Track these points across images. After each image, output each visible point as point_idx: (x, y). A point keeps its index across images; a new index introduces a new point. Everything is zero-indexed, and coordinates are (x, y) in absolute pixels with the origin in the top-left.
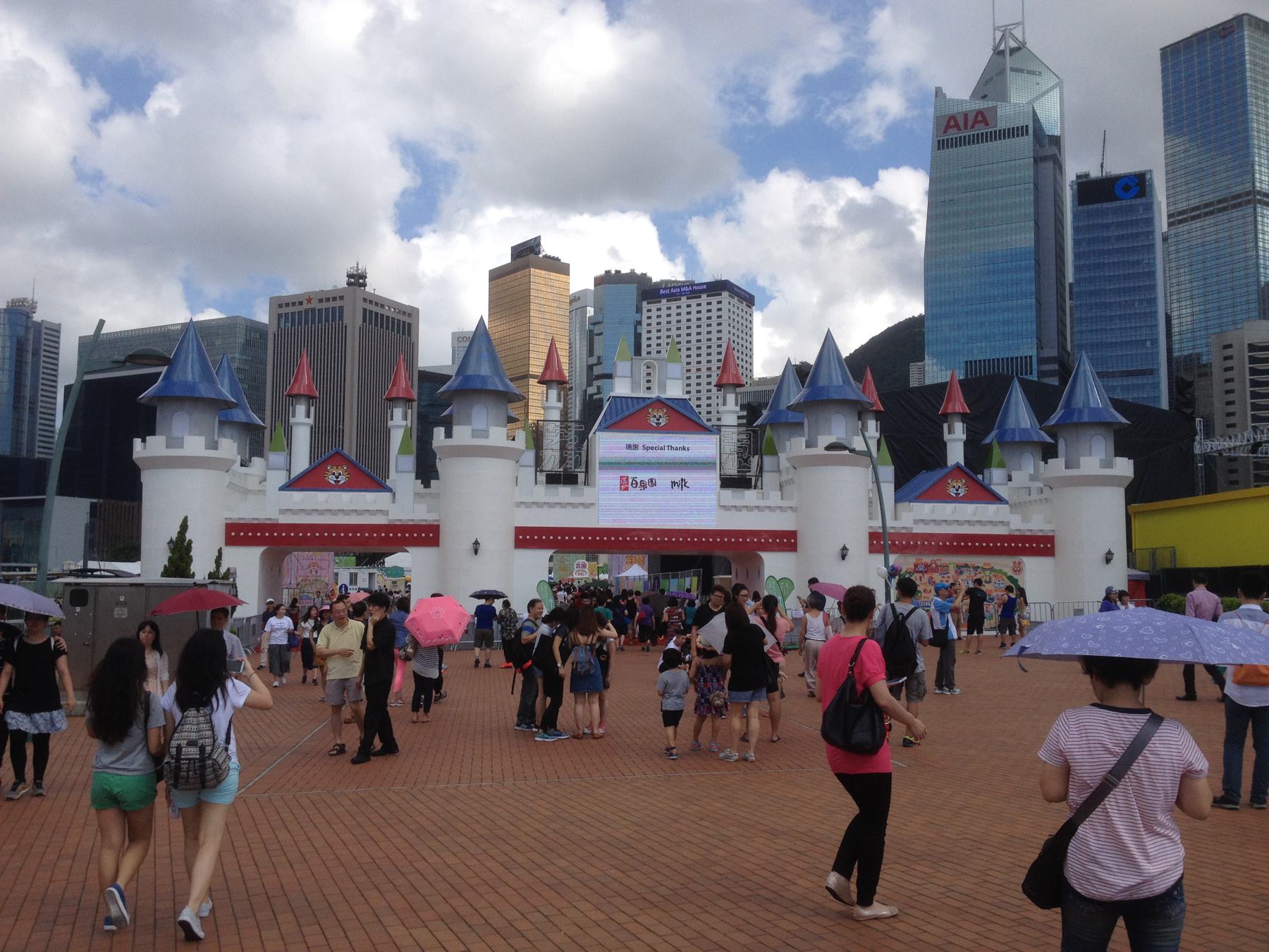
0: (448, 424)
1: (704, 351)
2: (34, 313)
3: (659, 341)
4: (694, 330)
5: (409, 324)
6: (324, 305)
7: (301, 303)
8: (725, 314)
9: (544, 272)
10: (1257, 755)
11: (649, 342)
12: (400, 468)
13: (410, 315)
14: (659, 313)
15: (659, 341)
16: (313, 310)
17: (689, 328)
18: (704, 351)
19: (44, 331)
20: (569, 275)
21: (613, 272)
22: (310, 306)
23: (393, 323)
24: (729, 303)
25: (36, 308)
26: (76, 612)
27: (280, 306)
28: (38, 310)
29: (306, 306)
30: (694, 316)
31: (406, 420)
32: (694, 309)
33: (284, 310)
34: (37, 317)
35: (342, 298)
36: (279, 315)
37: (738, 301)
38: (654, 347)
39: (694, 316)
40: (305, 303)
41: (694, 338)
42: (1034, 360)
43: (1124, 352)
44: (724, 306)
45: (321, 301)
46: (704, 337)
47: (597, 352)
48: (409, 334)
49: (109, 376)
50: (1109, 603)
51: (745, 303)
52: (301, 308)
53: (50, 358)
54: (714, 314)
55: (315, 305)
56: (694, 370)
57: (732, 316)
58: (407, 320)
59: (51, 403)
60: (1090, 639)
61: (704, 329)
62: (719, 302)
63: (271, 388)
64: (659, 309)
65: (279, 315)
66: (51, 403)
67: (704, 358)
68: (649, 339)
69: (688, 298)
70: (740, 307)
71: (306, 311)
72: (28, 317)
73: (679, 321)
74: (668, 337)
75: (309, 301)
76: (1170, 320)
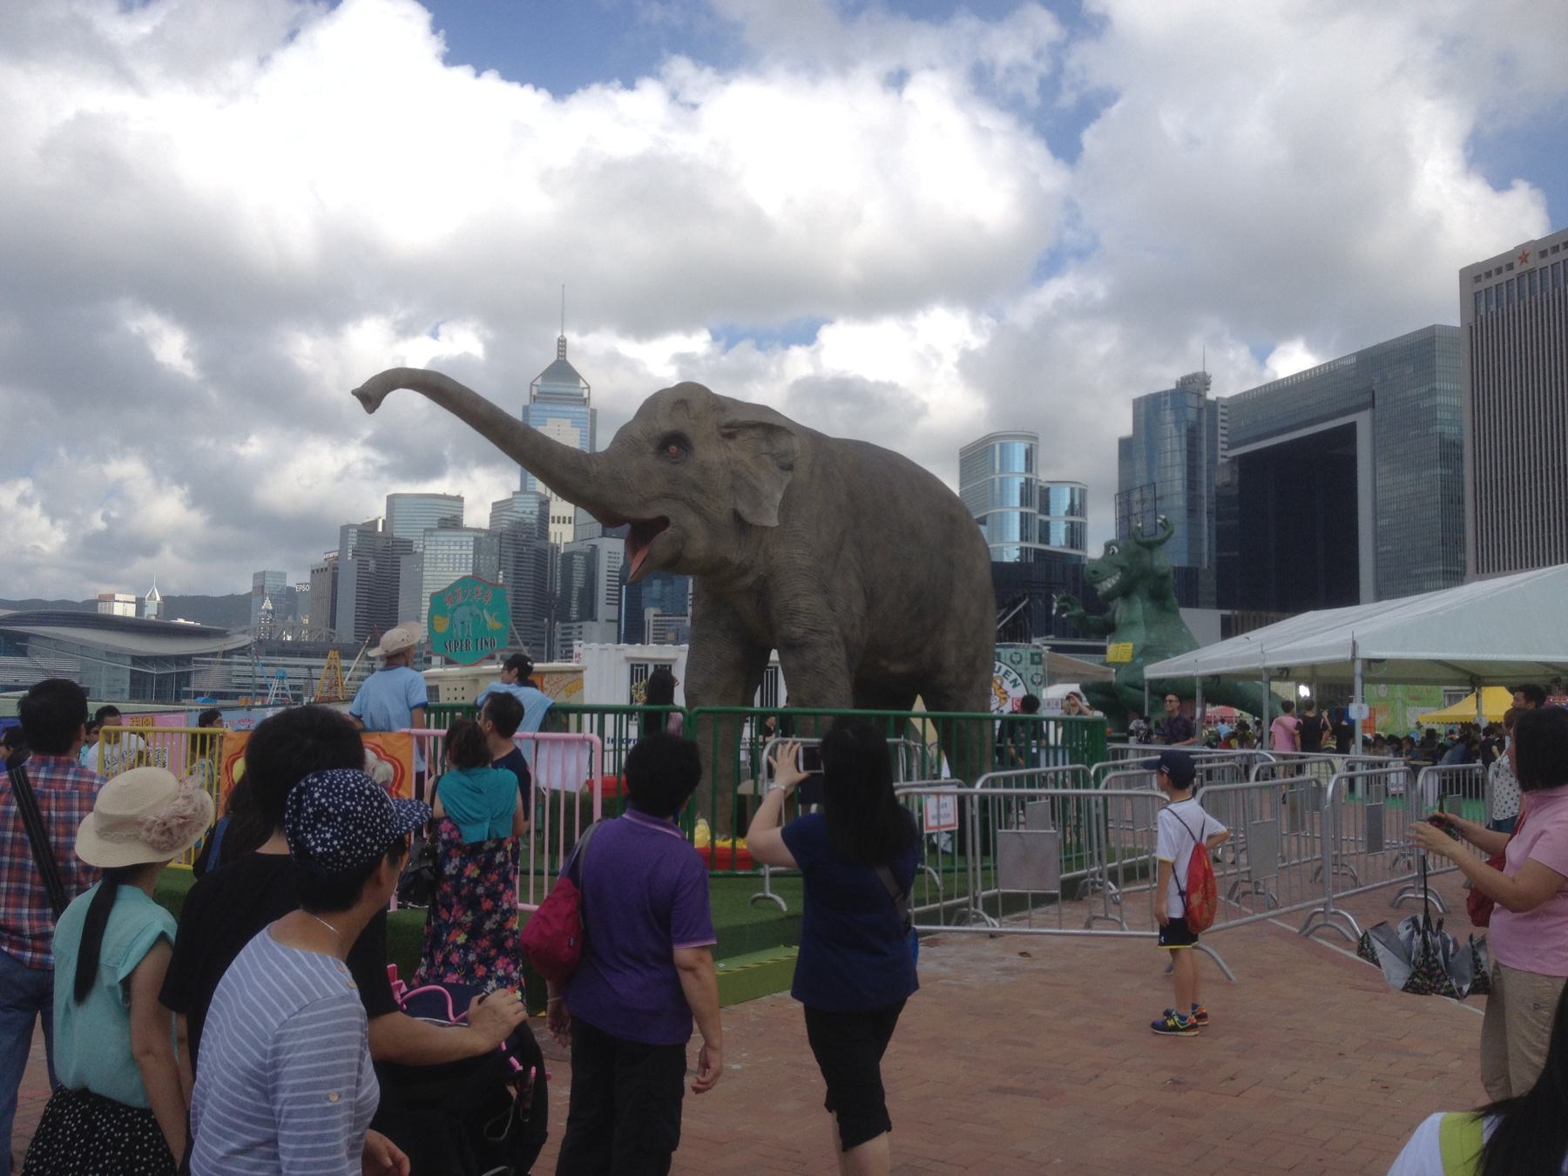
2: (1208, 389)
6: (1552, 259)
7: (1510, 267)
10: (388, 393)
16: (1531, 272)
19: (1220, 410)
22: (1526, 267)
25: (1209, 384)
27: (1478, 279)
28: (1212, 386)
29: (1518, 269)
31: (1271, 733)
34: (1211, 395)
36: (1476, 294)
40: (1517, 264)
42: (118, 728)
45: (1543, 254)
50: (562, 344)
52: (1512, 275)
53: (1552, 422)
55: (1535, 263)
59: (1556, 558)
63: (1472, 504)
66: (1556, 558)
71: (1520, 276)
72: (1200, 395)
76: (37, 809)
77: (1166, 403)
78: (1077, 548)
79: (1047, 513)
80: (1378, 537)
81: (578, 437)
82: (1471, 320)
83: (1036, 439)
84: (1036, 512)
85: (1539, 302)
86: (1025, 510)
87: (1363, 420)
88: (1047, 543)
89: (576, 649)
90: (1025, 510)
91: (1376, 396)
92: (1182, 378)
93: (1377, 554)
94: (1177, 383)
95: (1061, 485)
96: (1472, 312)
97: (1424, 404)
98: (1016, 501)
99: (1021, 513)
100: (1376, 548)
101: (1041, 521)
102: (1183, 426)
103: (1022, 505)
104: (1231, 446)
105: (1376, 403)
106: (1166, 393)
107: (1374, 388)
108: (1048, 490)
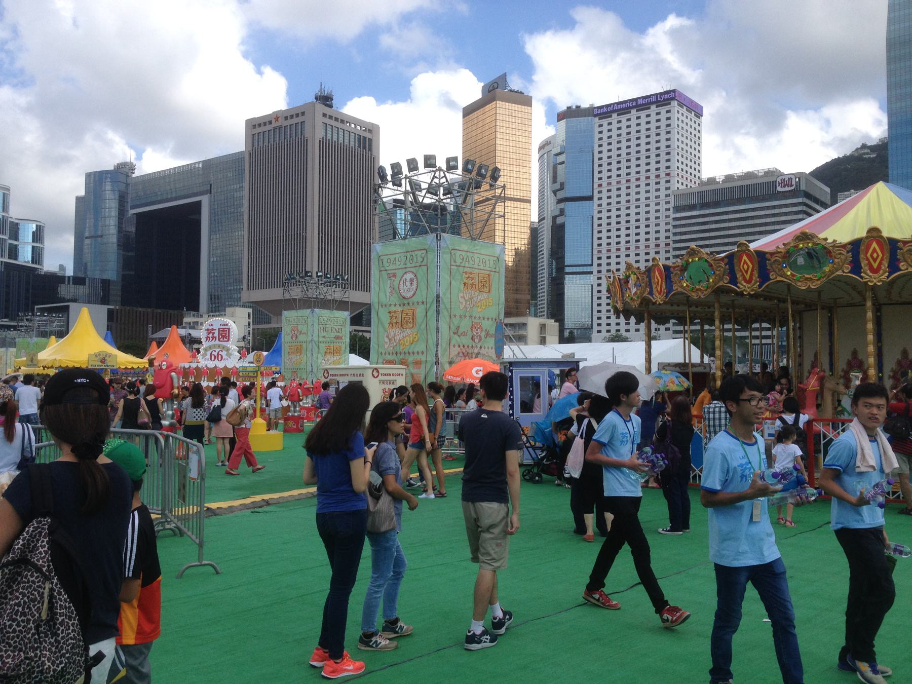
0: (682, 266)
1: (653, 159)
3: (609, 241)
4: (643, 141)
5: (370, 140)
6: (290, 122)
7: (270, 123)
8: (674, 122)
9: (515, 105)
11: (600, 156)
12: (590, 263)
13: (370, 131)
14: (609, 174)
15: (609, 241)
16: (280, 127)
17: (618, 223)
18: (653, 159)
20: (531, 106)
21: (574, 107)
23: (359, 139)
24: (678, 112)
26: (176, 404)
27: (254, 126)
29: (274, 124)
30: (643, 127)
32: (643, 120)
33: (258, 130)
35: (303, 113)
36: (253, 135)
37: (687, 110)
38: (605, 160)
39: (643, 127)
41: (643, 148)
43: (554, 272)
44: (675, 115)
45: (286, 118)
46: (653, 146)
47: (560, 179)
48: (370, 149)
49: (152, 209)
51: (693, 113)
54: (663, 123)
55: (281, 122)
56: (613, 250)
57: (681, 125)
58: (367, 135)
60: (865, 377)
61: (653, 139)
62: (668, 112)
64: (610, 124)
65: (253, 135)
67: (653, 167)
68: (600, 152)
69: (637, 111)
70: (689, 117)
71: (275, 129)
73: (629, 133)
74: (608, 271)
75: (277, 119)
77: (106, 178)
78: (36, 263)
79: (16, 239)
80: (210, 269)
81: (96, 277)
82: (250, 149)
83: (9, 190)
84: (7, 238)
85: (288, 143)
86: (35, 244)
87: (205, 200)
88: (16, 258)
89: (144, 670)
90: (35, 244)
91: (212, 187)
92: (118, 164)
93: (209, 276)
94: (115, 166)
95: (28, 222)
96: (250, 145)
97: (237, 195)
98: (30, 238)
99: (33, 247)
100: (209, 274)
101: (10, 244)
102: (117, 193)
103: (33, 241)
104: (133, 207)
105: (212, 192)
106: (107, 172)
107: (212, 182)
108: (17, 224)
